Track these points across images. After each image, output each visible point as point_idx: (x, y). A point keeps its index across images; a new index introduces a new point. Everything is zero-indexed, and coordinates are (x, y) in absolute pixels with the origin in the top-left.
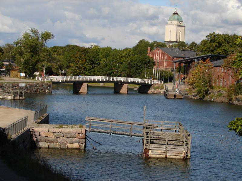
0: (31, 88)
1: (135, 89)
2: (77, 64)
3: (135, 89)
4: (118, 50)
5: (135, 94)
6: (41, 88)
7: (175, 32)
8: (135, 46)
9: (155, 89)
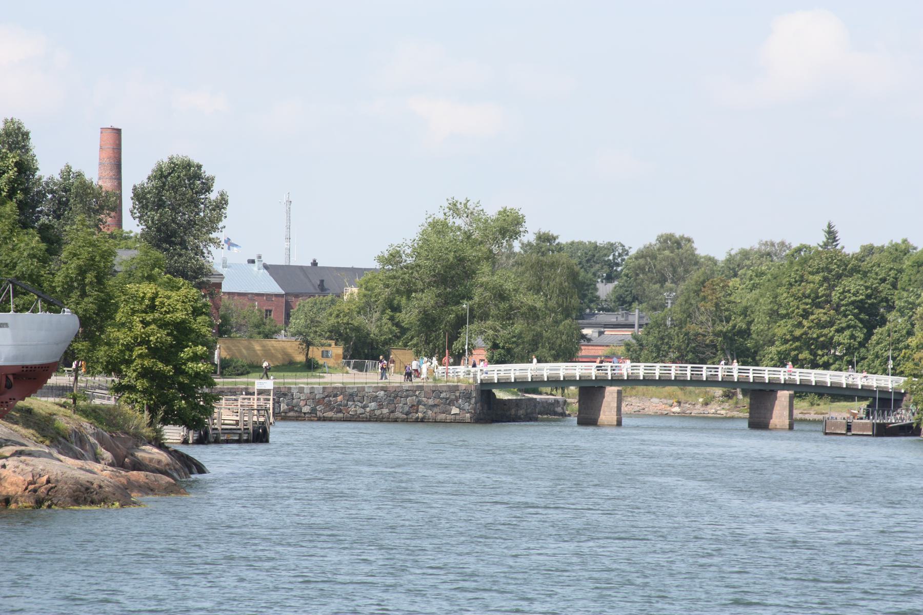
2: (800, 325)
4: (57, 177)
5: (330, 420)
6: (431, 402)
8: (714, 245)
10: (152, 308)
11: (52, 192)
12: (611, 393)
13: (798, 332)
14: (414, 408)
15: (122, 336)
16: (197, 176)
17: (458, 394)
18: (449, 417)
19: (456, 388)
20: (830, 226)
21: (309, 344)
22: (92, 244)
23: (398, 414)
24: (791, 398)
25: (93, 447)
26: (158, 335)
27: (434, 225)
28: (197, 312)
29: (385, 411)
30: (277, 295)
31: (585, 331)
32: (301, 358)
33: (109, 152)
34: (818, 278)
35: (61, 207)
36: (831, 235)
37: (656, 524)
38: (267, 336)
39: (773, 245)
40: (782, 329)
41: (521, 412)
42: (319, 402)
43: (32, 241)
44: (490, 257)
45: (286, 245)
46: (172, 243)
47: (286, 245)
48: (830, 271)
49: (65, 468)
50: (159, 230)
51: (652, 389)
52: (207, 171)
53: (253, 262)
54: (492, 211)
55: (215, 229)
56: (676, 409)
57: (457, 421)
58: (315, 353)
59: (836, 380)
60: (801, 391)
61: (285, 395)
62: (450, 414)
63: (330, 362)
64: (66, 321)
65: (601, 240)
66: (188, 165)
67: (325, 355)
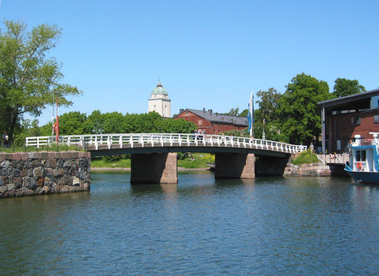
0: (17, 174)
1: (319, 171)
3: (319, 171)
6: (55, 172)
7: (161, 106)
9: (298, 163)
12: (172, 158)
17: (77, 163)
18: (71, 188)
23: (24, 190)
29: (11, 186)
37: (350, 263)
62: (72, 185)
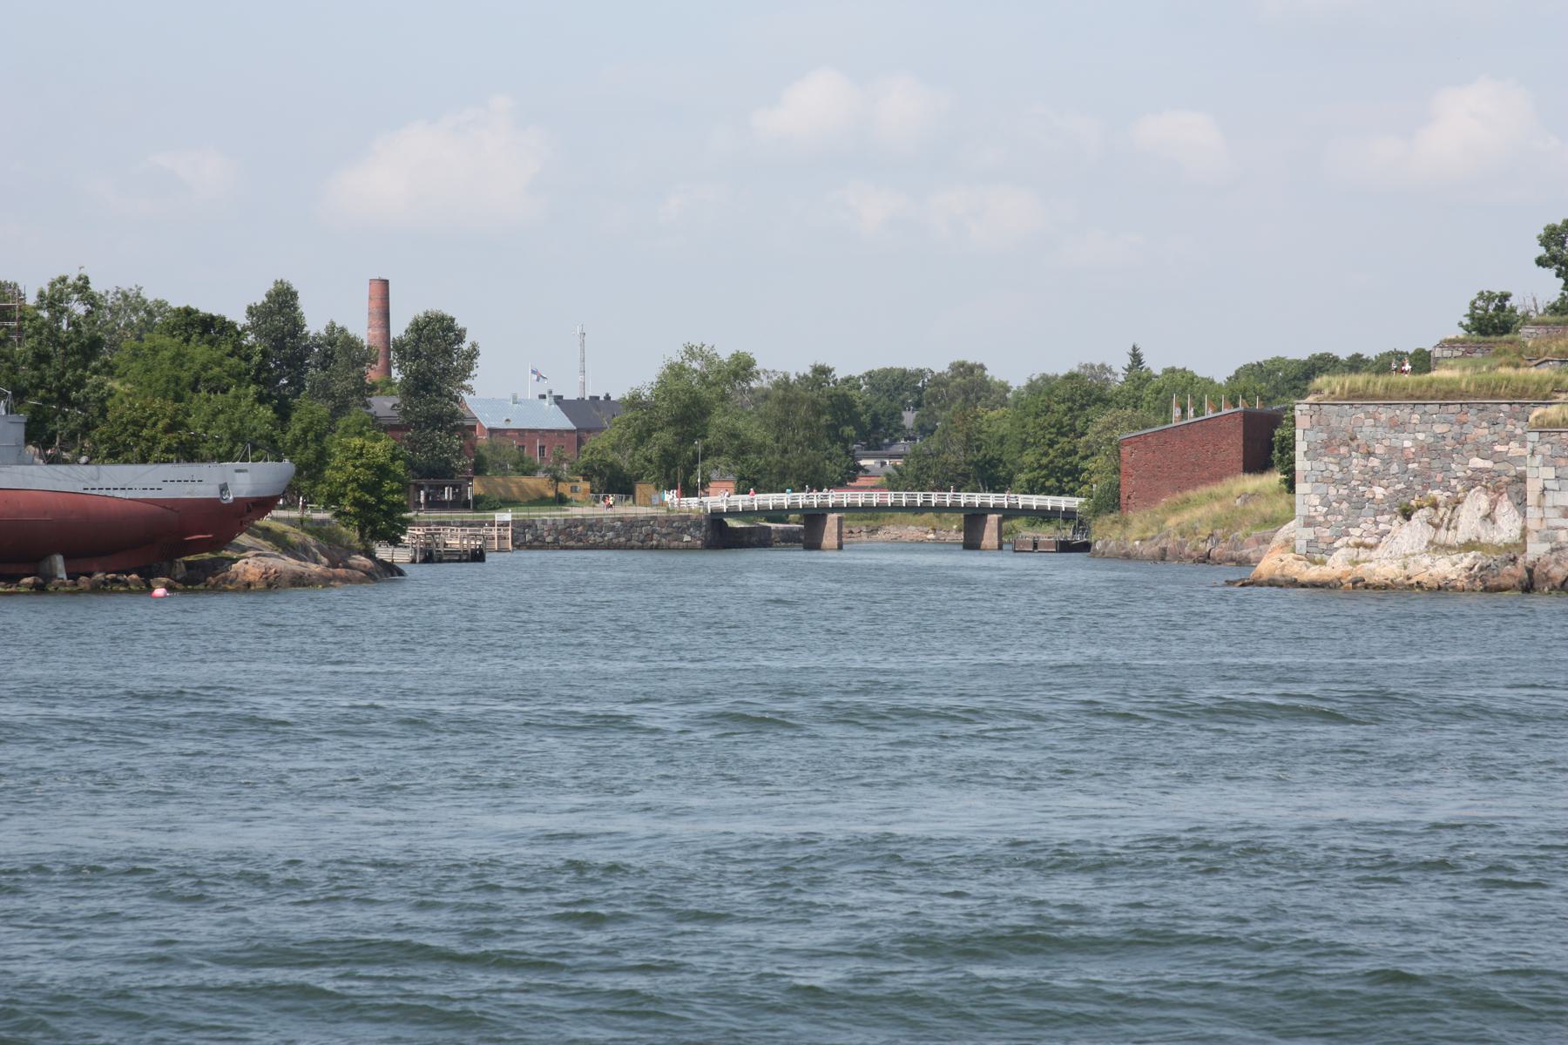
2: (1046, 454)
4: (323, 333)
5: (572, 548)
6: (664, 531)
10: (361, 455)
11: (318, 346)
13: (1044, 461)
14: (649, 536)
15: (340, 477)
16: (450, 328)
19: (688, 518)
20: (1134, 349)
21: (558, 480)
22: (312, 412)
23: (634, 542)
24: (1000, 521)
25: (315, 555)
26: (365, 476)
27: (671, 367)
28: (394, 458)
29: (622, 539)
30: (568, 431)
31: (862, 463)
32: (551, 494)
33: (377, 302)
34: (1063, 407)
35: (327, 359)
36: (1136, 357)
38: (525, 474)
39: (1092, 367)
40: (1029, 457)
41: (754, 539)
42: (560, 533)
43: (266, 412)
44: (724, 398)
45: (580, 378)
46: (428, 391)
47: (580, 378)
48: (1074, 402)
49: (289, 564)
50: (416, 379)
51: (910, 517)
52: (460, 323)
53: (543, 397)
54: (725, 355)
55: (467, 377)
56: (931, 536)
57: (689, 548)
58: (564, 488)
59: (1056, 504)
60: (1010, 513)
61: (529, 526)
63: (579, 497)
64: (287, 466)
65: (911, 366)
66: (441, 319)
67: (574, 489)
